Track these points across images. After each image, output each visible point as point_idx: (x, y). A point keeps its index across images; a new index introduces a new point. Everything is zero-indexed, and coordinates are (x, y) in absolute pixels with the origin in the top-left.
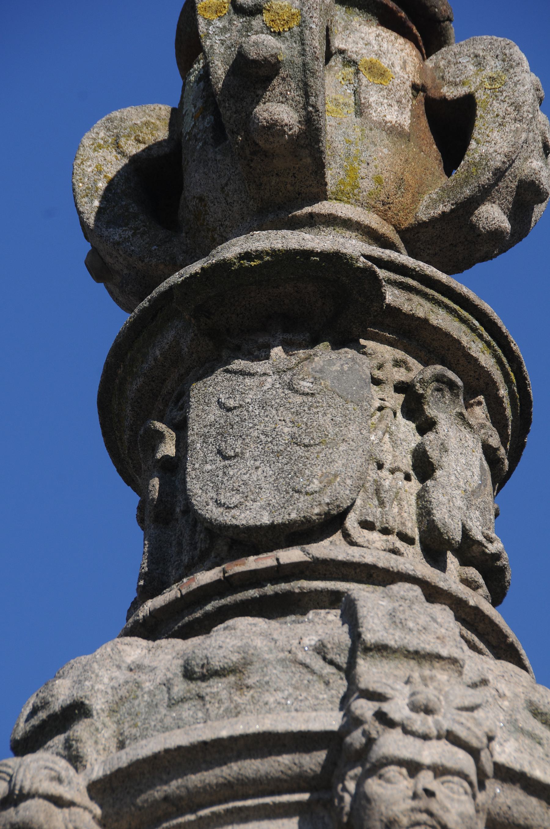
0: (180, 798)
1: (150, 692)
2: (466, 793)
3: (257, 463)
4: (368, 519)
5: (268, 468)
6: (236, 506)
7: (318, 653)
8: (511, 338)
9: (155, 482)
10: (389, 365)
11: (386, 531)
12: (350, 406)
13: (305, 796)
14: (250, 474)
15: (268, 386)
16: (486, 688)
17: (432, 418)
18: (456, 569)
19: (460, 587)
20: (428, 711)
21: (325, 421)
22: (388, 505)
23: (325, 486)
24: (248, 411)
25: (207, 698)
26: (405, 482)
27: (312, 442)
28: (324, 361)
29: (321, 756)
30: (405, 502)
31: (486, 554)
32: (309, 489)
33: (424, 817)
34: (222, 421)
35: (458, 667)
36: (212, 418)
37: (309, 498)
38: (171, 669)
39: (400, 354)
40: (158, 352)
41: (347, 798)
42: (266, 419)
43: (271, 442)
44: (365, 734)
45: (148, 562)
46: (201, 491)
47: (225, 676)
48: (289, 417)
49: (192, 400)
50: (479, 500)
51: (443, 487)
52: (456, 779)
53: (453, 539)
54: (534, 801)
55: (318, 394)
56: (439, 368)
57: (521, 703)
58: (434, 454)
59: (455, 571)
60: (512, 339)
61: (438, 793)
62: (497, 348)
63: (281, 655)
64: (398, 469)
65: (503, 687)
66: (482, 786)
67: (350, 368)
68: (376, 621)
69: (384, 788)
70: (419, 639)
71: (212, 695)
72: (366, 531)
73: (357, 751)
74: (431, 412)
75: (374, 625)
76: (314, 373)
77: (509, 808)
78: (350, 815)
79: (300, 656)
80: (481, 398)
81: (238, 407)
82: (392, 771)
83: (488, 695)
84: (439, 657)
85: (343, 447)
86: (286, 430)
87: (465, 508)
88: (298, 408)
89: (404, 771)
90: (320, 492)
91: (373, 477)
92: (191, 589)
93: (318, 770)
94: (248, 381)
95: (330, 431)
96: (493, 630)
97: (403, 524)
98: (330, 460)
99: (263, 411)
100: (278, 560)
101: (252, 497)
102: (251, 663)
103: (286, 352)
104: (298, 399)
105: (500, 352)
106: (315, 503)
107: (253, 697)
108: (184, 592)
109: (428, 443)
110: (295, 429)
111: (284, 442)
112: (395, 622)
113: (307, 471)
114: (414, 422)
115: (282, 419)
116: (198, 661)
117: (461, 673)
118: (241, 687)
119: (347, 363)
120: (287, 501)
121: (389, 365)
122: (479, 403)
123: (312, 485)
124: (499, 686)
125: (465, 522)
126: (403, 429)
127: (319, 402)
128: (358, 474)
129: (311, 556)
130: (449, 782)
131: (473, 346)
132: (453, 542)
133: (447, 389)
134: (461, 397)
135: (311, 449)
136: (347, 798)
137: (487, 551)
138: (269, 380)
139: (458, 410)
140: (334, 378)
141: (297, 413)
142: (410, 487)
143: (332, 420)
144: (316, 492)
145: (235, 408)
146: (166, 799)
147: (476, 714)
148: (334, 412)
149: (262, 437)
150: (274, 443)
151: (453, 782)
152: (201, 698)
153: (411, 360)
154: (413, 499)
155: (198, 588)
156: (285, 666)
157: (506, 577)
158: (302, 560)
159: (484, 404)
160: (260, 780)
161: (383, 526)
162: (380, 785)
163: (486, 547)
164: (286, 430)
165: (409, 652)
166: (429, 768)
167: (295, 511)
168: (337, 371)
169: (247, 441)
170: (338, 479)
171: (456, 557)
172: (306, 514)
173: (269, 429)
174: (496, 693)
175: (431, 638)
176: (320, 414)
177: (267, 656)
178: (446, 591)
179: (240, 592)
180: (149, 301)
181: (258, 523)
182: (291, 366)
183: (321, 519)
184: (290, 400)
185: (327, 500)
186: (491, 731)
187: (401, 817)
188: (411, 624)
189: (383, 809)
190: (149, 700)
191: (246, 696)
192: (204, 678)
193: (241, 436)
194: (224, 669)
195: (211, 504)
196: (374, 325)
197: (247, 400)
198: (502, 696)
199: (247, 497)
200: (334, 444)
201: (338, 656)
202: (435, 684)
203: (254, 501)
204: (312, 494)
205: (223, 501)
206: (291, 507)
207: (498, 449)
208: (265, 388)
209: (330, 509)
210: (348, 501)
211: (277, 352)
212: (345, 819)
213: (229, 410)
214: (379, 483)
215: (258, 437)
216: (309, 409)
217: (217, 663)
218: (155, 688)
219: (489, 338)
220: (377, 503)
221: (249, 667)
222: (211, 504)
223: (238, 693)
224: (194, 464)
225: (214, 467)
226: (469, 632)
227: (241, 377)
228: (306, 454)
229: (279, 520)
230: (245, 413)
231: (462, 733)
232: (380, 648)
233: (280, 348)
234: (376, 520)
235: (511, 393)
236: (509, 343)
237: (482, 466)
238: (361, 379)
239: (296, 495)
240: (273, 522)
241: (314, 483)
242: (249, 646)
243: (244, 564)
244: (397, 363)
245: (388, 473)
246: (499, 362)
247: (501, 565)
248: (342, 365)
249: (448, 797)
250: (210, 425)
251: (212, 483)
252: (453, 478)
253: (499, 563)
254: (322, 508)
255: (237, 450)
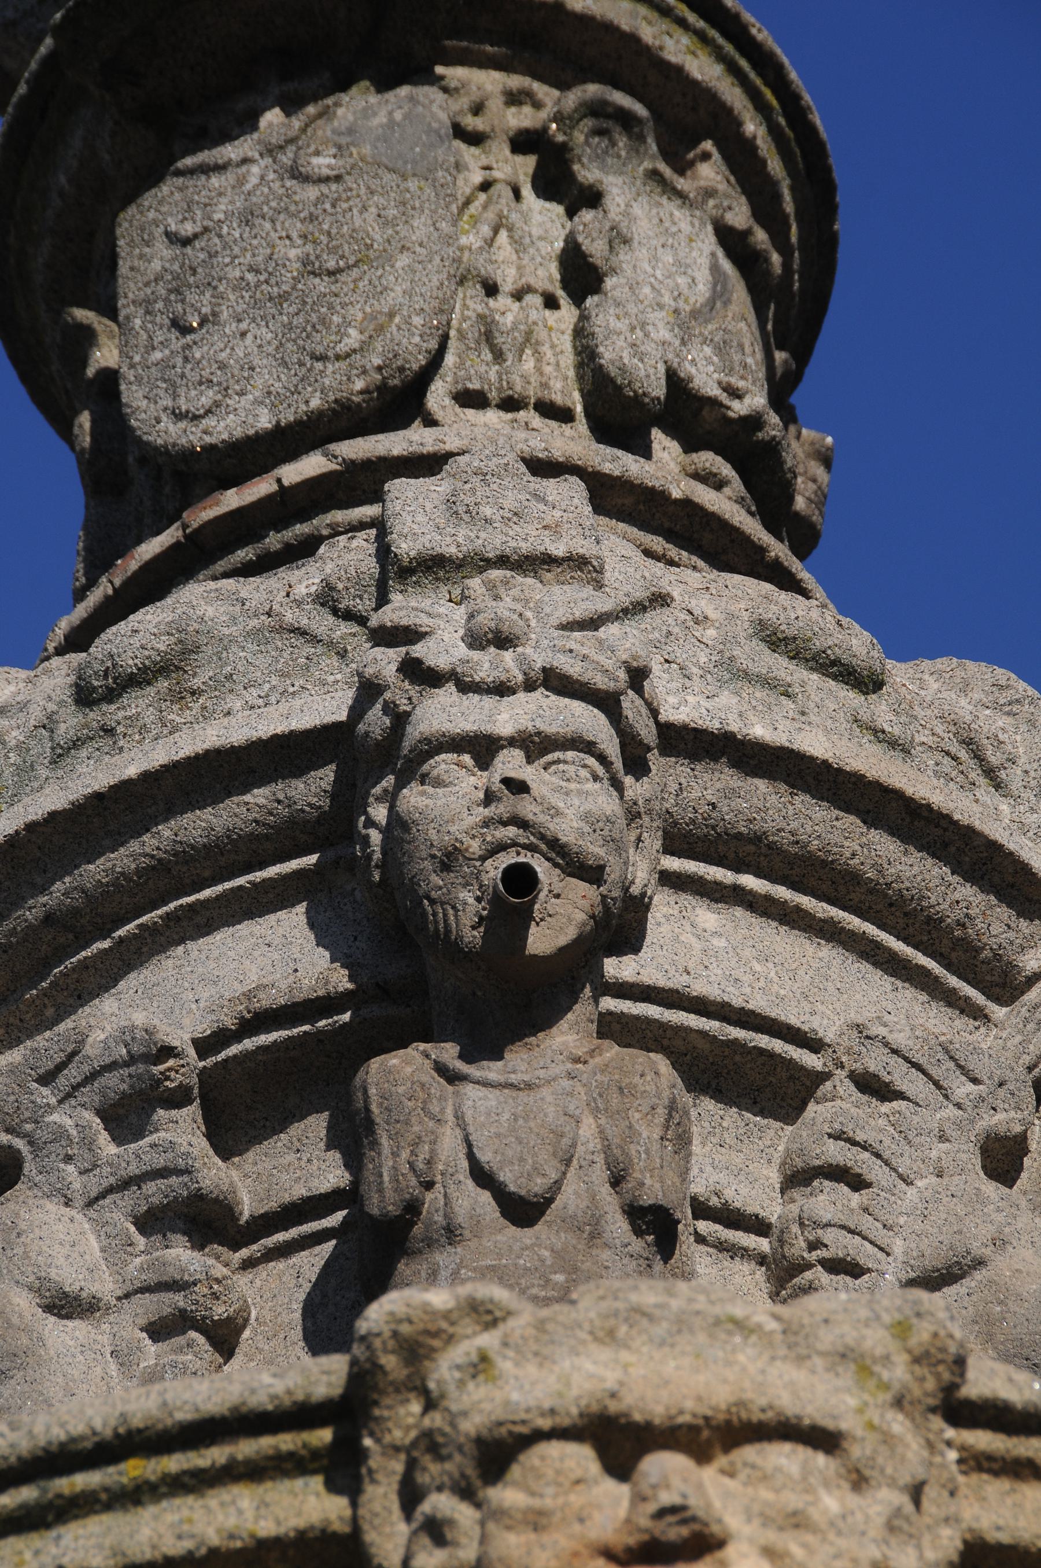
0: (75, 912)
1: (19, 747)
2: (596, 778)
3: (244, 326)
4: (470, 386)
5: (264, 330)
6: (209, 412)
7: (322, 605)
8: (748, 17)
9: (85, 419)
10: (495, 104)
11: (511, 404)
12: (412, 184)
13: (313, 859)
14: (233, 349)
15: (254, 180)
16: (666, 611)
17: (591, 187)
18: (673, 459)
19: (647, 468)
20: (503, 641)
21: (367, 222)
22: (510, 357)
23: (371, 337)
24: (220, 236)
25: (120, 729)
26: (547, 313)
27: (341, 263)
28: (354, 113)
29: (326, 776)
30: (547, 345)
31: (731, 421)
32: (342, 348)
33: (512, 831)
34: (176, 267)
35: (589, 572)
36: (156, 265)
37: (343, 365)
38: (53, 695)
39: (516, 81)
40: (63, 179)
41: (375, 837)
42: (255, 242)
43: (267, 282)
44: (389, 708)
45: (85, 568)
46: (145, 402)
47: (149, 683)
48: (296, 228)
49: (121, 243)
50: (710, 327)
51: (618, 304)
52: (570, 755)
53: (644, 394)
54: (761, 785)
55: (349, 174)
56: (592, 90)
57: (743, 627)
58: (595, 248)
59: (672, 465)
60: (752, 20)
61: (533, 785)
62: (721, 40)
63: (254, 623)
64: (528, 289)
65: (703, 605)
66: (637, 766)
67: (406, 117)
68: (420, 518)
69: (430, 797)
70: (506, 535)
71: (129, 722)
72: (470, 413)
73: (378, 744)
74: (589, 175)
75: (415, 526)
76: (336, 138)
77: (714, 806)
78: (383, 865)
79: (290, 617)
80: (708, 145)
81: (202, 234)
82: (443, 764)
83: (671, 621)
84: (548, 561)
85: (403, 261)
86: (293, 253)
87: (677, 343)
88: (312, 209)
89: (467, 758)
90: (362, 349)
91: (474, 310)
92: (129, 574)
93: (325, 803)
94: (215, 181)
95: (377, 237)
96: (732, 541)
97: (545, 386)
98: (379, 289)
99: (248, 229)
100: (279, 481)
101: (237, 387)
102: (196, 649)
103: (288, 114)
104: (312, 192)
105: (729, 48)
106: (355, 372)
107: (204, 708)
108: (117, 582)
109: (581, 228)
110: (309, 248)
111: (289, 275)
112: (456, 513)
113: (335, 318)
114: (560, 202)
115: (284, 234)
116: (96, 666)
117: (599, 586)
118: (180, 696)
119: (400, 107)
120: (302, 380)
121: (495, 104)
122: (706, 156)
123: (346, 340)
124: (693, 605)
125: (675, 365)
126: (537, 218)
127: (351, 190)
128: (435, 303)
129: (340, 459)
130: (558, 762)
131: (669, 43)
132: (647, 400)
133: (618, 129)
134: (651, 141)
135: (342, 277)
136: (375, 837)
137: (731, 414)
138: (255, 169)
139: (647, 165)
140: (378, 139)
141: (312, 218)
142: (559, 320)
143: (379, 216)
144: (354, 351)
145: (196, 236)
146: (49, 919)
147: (602, 633)
148: (382, 200)
149: (250, 277)
150: (273, 281)
151: (565, 762)
152: (109, 731)
153: (540, 89)
154: (566, 342)
155: (140, 568)
156: (264, 641)
157: (785, 462)
158: (324, 470)
159: (716, 155)
160: (217, 846)
161: (503, 395)
162: (423, 793)
163: (728, 408)
164: (293, 253)
165: (487, 560)
166: (512, 742)
167: (318, 394)
168: (382, 126)
169: (221, 289)
170: (397, 320)
171: (673, 438)
172: (339, 395)
173: (260, 258)
174: (689, 617)
175: (531, 529)
176: (355, 211)
177: (226, 631)
178: (618, 478)
179: (221, 558)
180: (27, 82)
181: (251, 432)
182: (291, 134)
183: (371, 399)
184: (297, 198)
185: (377, 361)
186: (635, 658)
187: (467, 840)
188: (487, 511)
189: (433, 834)
190: (19, 760)
191: (190, 709)
192: (111, 695)
193: (209, 284)
194: (143, 670)
195: (164, 418)
196: (458, 35)
197: (217, 216)
198: (701, 620)
199: (226, 389)
200: (386, 258)
201: (358, 600)
202: (514, 592)
203: (241, 393)
204: (348, 355)
205: (184, 408)
206: (309, 389)
207: (748, 232)
208: (248, 187)
209: (384, 378)
210: (420, 357)
211: (273, 117)
212: (377, 877)
213: (186, 242)
214: (489, 320)
215: (242, 278)
216: (334, 206)
217: (131, 662)
218: (27, 738)
219: (701, 24)
220: (489, 357)
221: (193, 656)
222: (164, 418)
223: (176, 707)
224: (131, 358)
225: (167, 352)
226: (685, 554)
227: (203, 178)
228: (333, 288)
229: (288, 416)
230: (216, 240)
231: (573, 668)
232: (430, 563)
233: (277, 110)
234: (486, 387)
235: (774, 130)
236: (744, 28)
237: (715, 268)
238: (430, 131)
239: (319, 365)
240: (278, 422)
241: (349, 336)
242: (189, 618)
243: (217, 504)
244: (514, 98)
245: (509, 301)
246: (733, 69)
247: (767, 438)
248: (390, 113)
249: (558, 789)
250: (156, 280)
251: (165, 381)
252: (647, 290)
253: (760, 435)
254: (368, 379)
255: (204, 310)
